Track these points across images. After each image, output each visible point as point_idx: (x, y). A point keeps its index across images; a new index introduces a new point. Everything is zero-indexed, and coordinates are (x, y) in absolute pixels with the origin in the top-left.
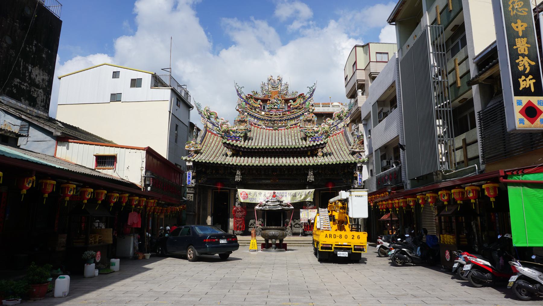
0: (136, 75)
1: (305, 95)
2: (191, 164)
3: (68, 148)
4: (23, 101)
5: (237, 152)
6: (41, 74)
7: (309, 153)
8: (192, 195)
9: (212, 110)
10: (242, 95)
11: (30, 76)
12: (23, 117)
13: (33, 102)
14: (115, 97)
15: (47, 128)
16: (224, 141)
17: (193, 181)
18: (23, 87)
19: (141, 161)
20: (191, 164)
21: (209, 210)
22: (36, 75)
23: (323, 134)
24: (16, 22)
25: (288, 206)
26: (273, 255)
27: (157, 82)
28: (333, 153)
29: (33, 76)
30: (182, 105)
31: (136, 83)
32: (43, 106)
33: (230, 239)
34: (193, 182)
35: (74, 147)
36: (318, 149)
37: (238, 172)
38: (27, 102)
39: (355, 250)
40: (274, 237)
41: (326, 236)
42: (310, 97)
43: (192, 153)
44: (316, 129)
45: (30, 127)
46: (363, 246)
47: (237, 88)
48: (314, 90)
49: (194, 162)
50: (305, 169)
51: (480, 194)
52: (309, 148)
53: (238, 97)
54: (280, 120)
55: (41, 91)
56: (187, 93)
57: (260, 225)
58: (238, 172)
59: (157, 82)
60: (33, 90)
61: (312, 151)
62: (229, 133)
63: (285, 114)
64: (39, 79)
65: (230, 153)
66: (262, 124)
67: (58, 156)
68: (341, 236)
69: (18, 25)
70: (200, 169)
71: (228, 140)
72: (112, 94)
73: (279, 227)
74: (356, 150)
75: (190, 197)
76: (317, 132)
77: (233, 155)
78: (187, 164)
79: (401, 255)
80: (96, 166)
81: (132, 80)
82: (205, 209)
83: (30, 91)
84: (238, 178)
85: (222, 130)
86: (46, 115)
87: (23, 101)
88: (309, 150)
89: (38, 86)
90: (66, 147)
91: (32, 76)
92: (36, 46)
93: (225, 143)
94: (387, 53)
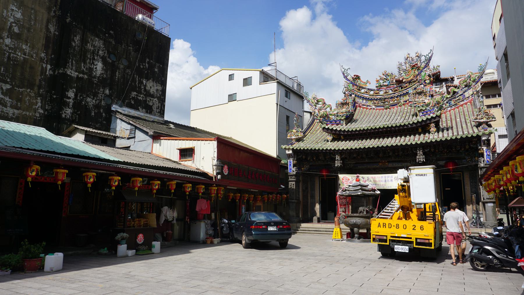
0: (246, 74)
2: (291, 152)
3: (160, 145)
4: (140, 109)
5: (338, 136)
6: (155, 85)
7: (420, 130)
8: (294, 183)
9: (319, 98)
11: (145, 88)
12: (131, 122)
13: (149, 110)
14: (232, 98)
15: (145, 129)
16: (323, 126)
17: (294, 169)
18: (140, 98)
19: (213, 151)
20: (291, 152)
21: (317, 197)
22: (151, 87)
23: (435, 106)
24: (130, 46)
25: (374, 190)
28: (452, 128)
29: (148, 88)
30: (292, 96)
31: (247, 82)
32: (158, 112)
33: (281, 227)
34: (294, 170)
35: (165, 143)
36: (430, 123)
37: (338, 157)
38: (144, 110)
39: (417, 244)
40: (359, 227)
41: (379, 225)
43: (294, 141)
44: (426, 101)
45: (137, 130)
46: (429, 240)
47: (343, 70)
49: (293, 149)
50: (413, 148)
52: (419, 125)
53: (345, 80)
54: (392, 98)
55: (156, 99)
56: (299, 85)
57: (343, 212)
58: (338, 157)
59: (266, 77)
60: (148, 99)
61: (422, 128)
62: (329, 117)
63: (396, 90)
64: (153, 90)
65: (330, 138)
66: (371, 105)
67: (154, 152)
68: (398, 226)
69: (131, 48)
71: (327, 125)
72: (229, 95)
74: (482, 120)
75: (292, 185)
76: (428, 105)
77: (333, 140)
78: (287, 152)
79: (483, 255)
80: (180, 159)
81: (244, 79)
82: (313, 197)
83: (146, 101)
84: (338, 164)
85: (320, 115)
86: (162, 119)
87: (140, 109)
88: (420, 126)
89: (152, 96)
90: (158, 144)
91: (147, 88)
92: (148, 63)
93: (324, 128)
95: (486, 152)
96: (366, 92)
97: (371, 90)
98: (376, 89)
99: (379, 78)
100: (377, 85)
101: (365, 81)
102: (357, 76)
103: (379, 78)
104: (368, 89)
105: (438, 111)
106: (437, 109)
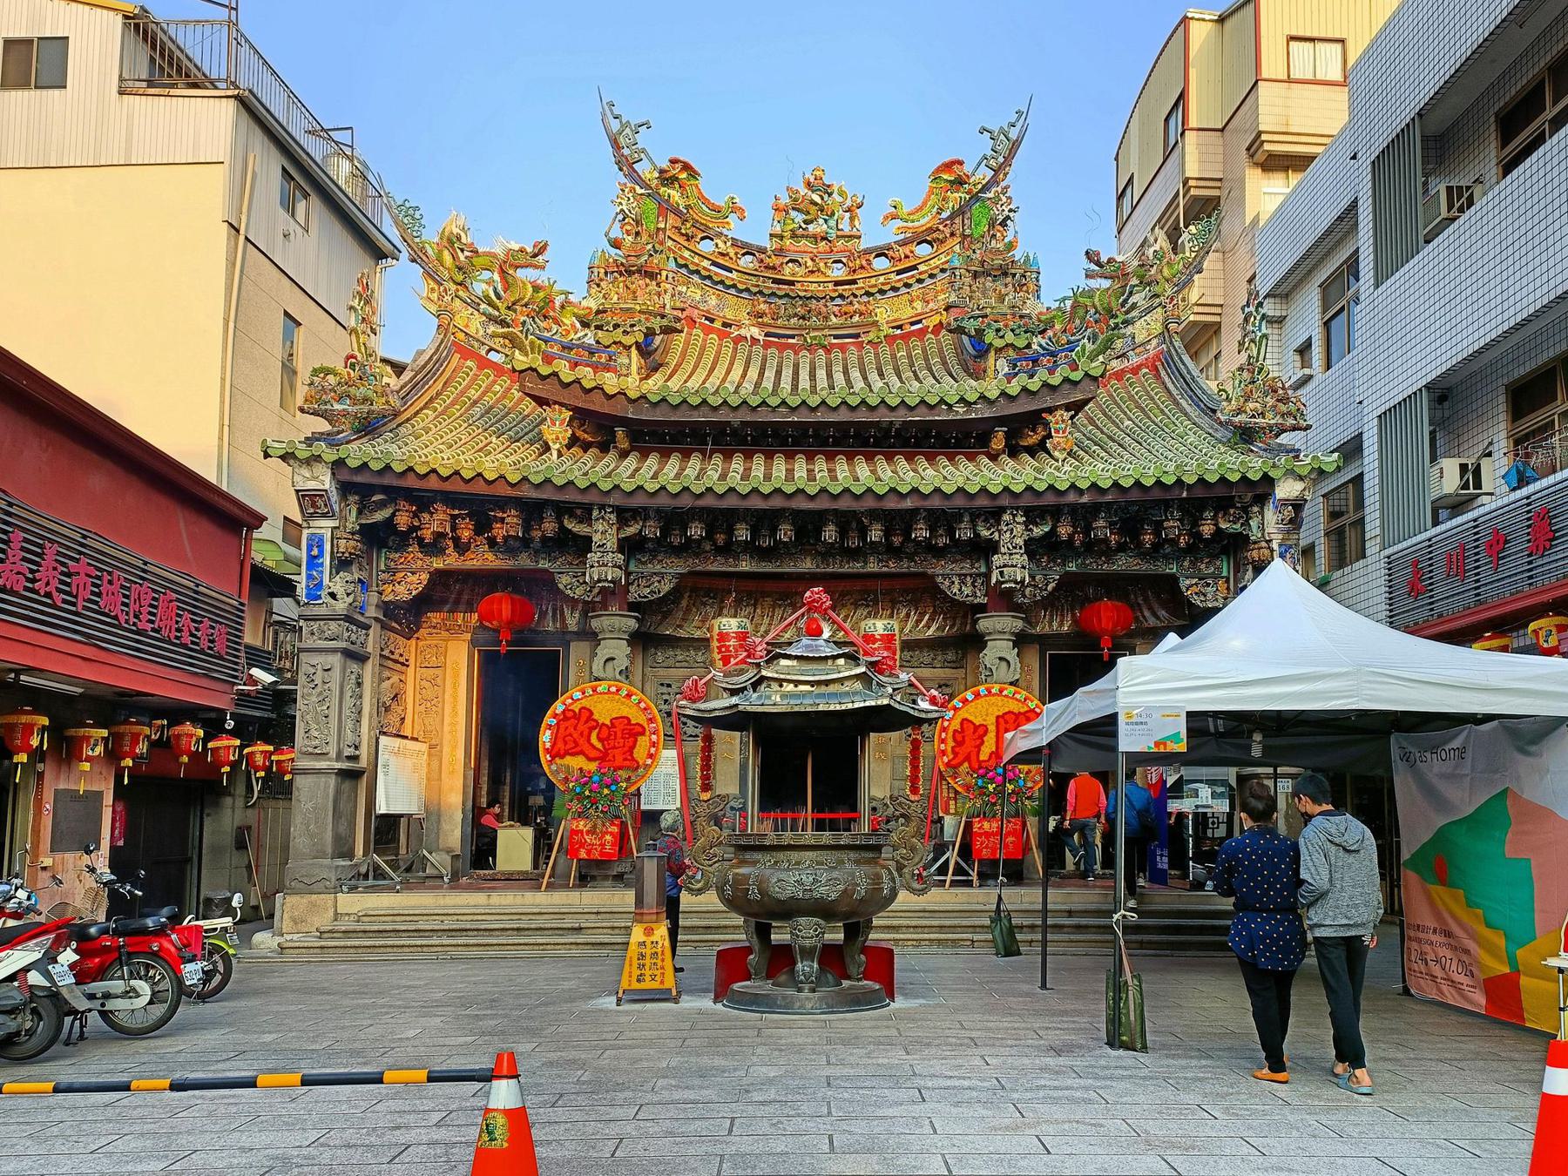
1: (968, 168)
5: (600, 427)
7: (998, 442)
10: (644, 169)
26: (805, 1034)
27: (161, 63)
42: (994, 182)
48: (1015, 145)
51: (196, 945)
58: (604, 533)
59: (161, 63)
61: (1021, 430)
70: (379, 516)
73: (845, 838)
94: (1342, 41)
97: (749, 250)
99: (785, 200)
100: (778, 229)
102: (686, 167)
103: (785, 200)
104: (735, 243)
105: (1092, 358)
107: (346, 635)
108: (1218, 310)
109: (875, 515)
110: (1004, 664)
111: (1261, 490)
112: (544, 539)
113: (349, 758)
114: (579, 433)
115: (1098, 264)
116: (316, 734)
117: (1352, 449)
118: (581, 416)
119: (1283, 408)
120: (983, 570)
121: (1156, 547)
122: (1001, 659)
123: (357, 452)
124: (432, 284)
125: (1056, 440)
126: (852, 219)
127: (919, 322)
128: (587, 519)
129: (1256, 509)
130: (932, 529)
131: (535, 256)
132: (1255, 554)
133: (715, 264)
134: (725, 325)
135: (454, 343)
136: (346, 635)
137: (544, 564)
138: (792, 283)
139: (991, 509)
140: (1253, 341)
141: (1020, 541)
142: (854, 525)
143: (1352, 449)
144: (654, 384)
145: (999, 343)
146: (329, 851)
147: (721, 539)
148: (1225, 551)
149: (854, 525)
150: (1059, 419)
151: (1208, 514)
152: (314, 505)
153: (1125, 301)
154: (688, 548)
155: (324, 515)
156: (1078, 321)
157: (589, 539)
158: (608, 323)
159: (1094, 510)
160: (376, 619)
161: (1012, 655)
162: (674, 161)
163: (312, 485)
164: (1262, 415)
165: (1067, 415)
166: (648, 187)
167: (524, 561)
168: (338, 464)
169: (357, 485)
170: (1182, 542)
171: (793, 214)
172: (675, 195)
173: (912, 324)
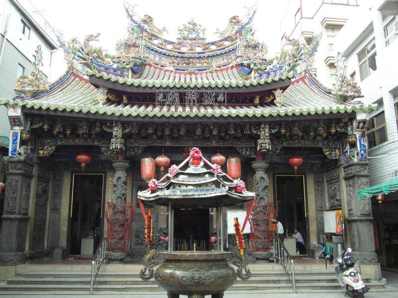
5: (117, 94)
7: (257, 101)
58: (117, 131)
61: (265, 95)
95: (360, 140)
96: (161, 44)
97: (171, 43)
98: (176, 41)
99: (182, 27)
100: (179, 36)
101: (160, 28)
102: (149, 17)
104: (165, 41)
105: (289, 71)
106: (288, 68)
107: (24, 168)
108: (315, 70)
109: (214, 124)
110: (262, 180)
111: (352, 116)
112: (96, 134)
113: (23, 214)
114: (110, 97)
115: (290, 41)
116: (11, 205)
117: (380, 102)
118: (110, 91)
119: (355, 90)
120: (254, 145)
121: (315, 137)
122: (261, 177)
123: (30, 103)
124: (66, 54)
125: (277, 100)
126: (203, 33)
127: (226, 65)
128: (111, 128)
129: (349, 123)
130: (235, 130)
131: (96, 37)
132: (350, 139)
133: (158, 47)
134: (162, 66)
135: (72, 73)
136: (24, 168)
137: (96, 143)
138: (184, 53)
139: (257, 122)
140: (341, 68)
141: (267, 134)
142: (207, 129)
143: (380, 102)
144: (137, 82)
145: (255, 68)
146: (14, 249)
147: (159, 134)
148: (338, 139)
149: (207, 129)
150: (278, 93)
151: (334, 125)
152: (15, 122)
153: (299, 53)
154: (146, 137)
155: (18, 125)
156: (283, 60)
157: (112, 134)
158: (121, 61)
159: (293, 122)
160: (37, 163)
161: (265, 176)
162: (145, 16)
163: (14, 114)
164: (347, 92)
165: (281, 91)
166: (137, 23)
167: (89, 142)
168: (24, 107)
169: (30, 114)
170: (324, 135)
171: (184, 32)
172: (146, 26)
173: (224, 66)
